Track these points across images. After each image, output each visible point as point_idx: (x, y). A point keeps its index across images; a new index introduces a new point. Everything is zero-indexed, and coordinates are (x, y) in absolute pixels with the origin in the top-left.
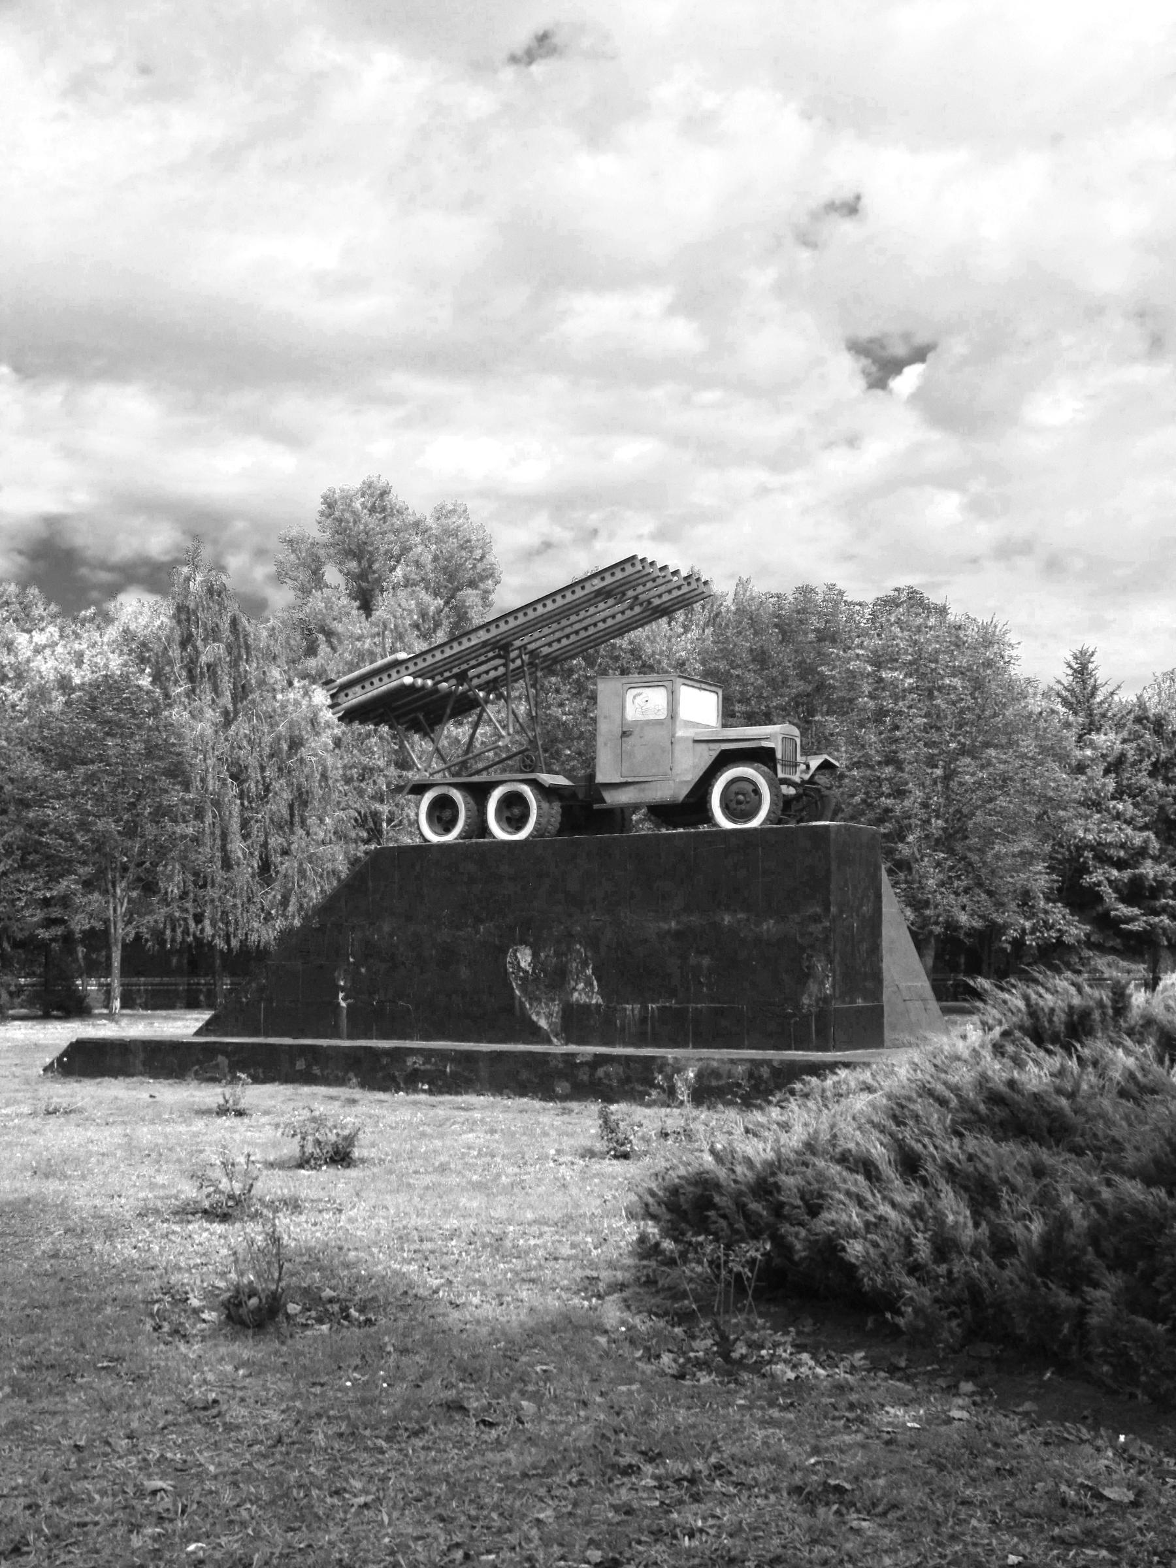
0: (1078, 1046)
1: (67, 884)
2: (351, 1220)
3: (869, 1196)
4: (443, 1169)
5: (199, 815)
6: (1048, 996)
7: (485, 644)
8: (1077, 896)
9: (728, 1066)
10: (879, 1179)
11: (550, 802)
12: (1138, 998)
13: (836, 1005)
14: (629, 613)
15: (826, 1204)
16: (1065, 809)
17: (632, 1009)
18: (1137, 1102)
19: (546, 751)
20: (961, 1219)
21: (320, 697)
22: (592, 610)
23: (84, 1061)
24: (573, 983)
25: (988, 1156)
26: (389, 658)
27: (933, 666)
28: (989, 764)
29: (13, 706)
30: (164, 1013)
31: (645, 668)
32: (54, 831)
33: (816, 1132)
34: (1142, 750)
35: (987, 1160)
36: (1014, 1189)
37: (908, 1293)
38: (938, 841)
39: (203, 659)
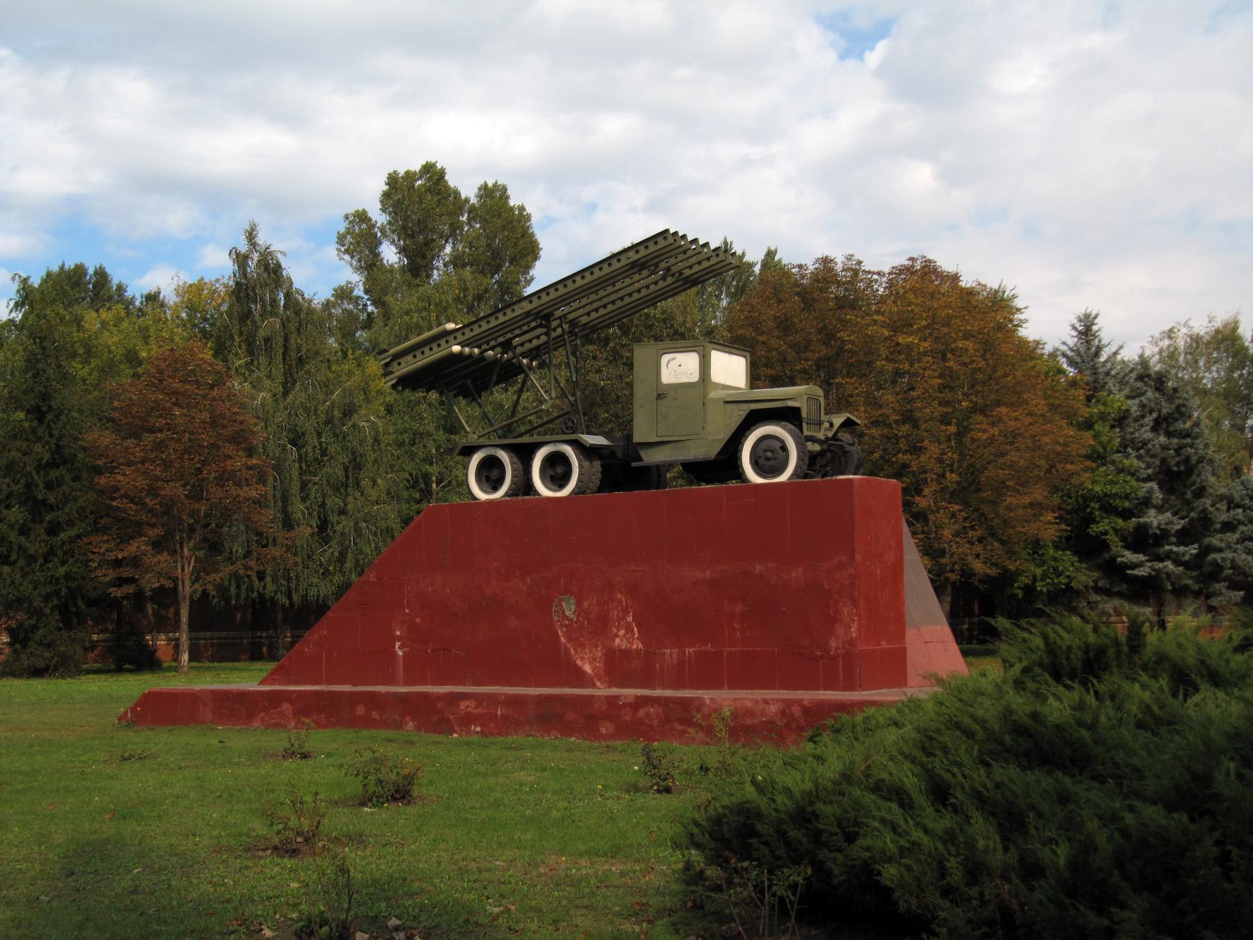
0: (1095, 681)
1: (137, 546)
2: (414, 854)
3: (902, 822)
4: (497, 804)
5: (262, 480)
6: (1064, 634)
7: (528, 314)
8: (1086, 545)
9: (762, 706)
10: (911, 808)
11: (591, 461)
12: (1152, 638)
13: (861, 647)
14: (661, 284)
15: (862, 832)
16: (1072, 463)
17: (671, 654)
18: (1154, 733)
19: (585, 414)
20: (991, 843)
21: (374, 366)
22: (628, 281)
23: (158, 711)
24: (615, 630)
25: (1015, 783)
26: (436, 330)
27: (946, 330)
28: (1000, 420)
29: (84, 381)
30: (230, 665)
31: (679, 338)
32: (125, 496)
33: (852, 762)
34: (1143, 406)
35: (1015, 788)
36: (1040, 815)
37: (942, 914)
38: (952, 493)
39: (261, 333)
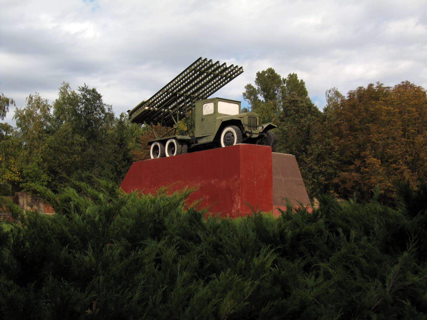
11: (182, 145)
